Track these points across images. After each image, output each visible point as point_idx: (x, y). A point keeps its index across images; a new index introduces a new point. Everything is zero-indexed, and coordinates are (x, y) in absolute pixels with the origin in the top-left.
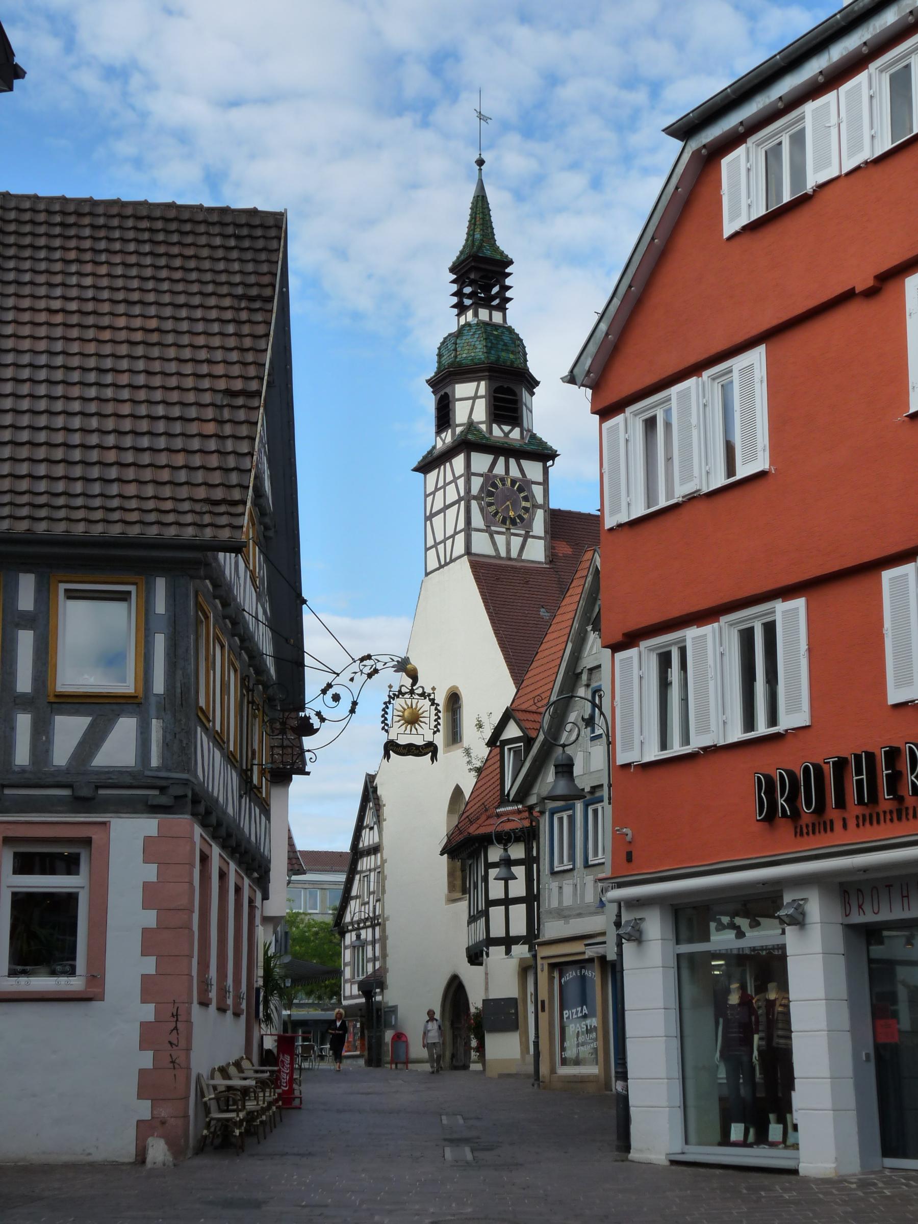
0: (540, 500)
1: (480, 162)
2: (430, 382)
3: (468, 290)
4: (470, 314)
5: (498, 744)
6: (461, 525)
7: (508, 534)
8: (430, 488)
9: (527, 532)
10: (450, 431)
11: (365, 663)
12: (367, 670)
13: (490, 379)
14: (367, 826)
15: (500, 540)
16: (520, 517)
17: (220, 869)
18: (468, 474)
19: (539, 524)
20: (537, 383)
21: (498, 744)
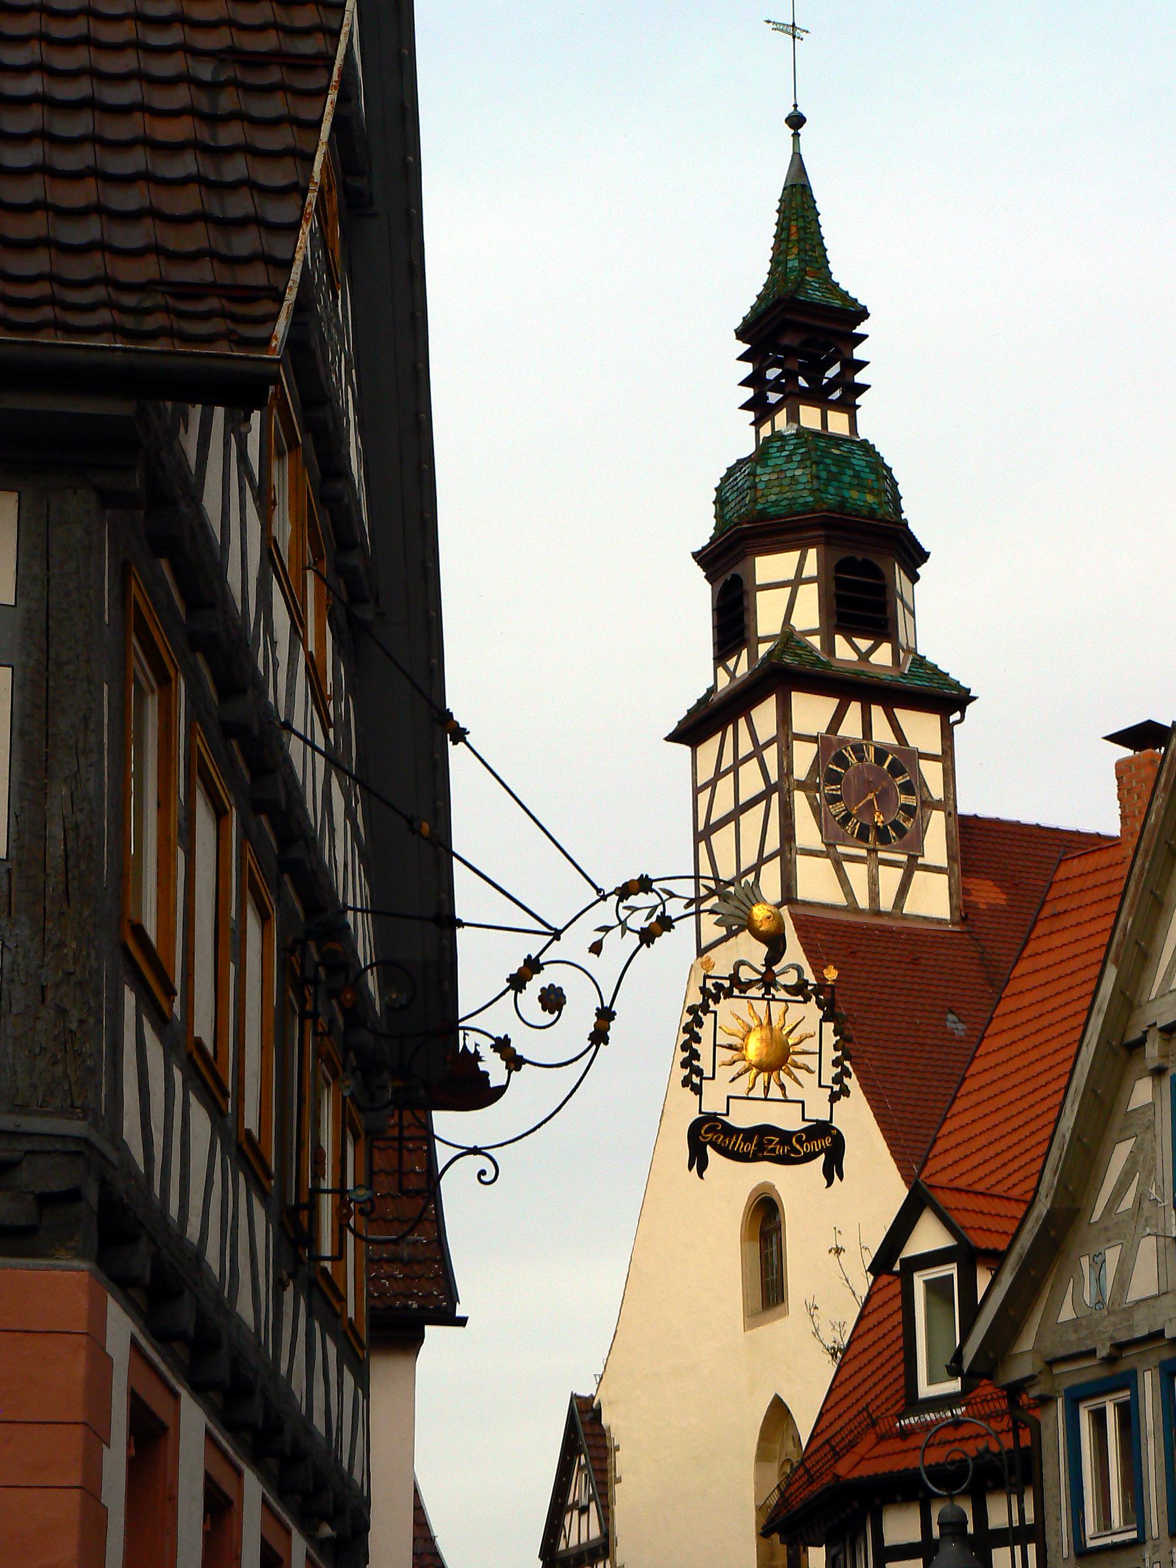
0: (937, 791)
1: (796, 121)
2: (701, 557)
3: (772, 373)
4: (781, 418)
5: (897, 1267)
6: (773, 842)
7: (874, 862)
8: (706, 773)
9: (913, 858)
10: (745, 652)
11: (633, 901)
12: (638, 921)
13: (826, 545)
14: (575, 1505)
15: (857, 874)
16: (896, 825)
17: (210, 1483)
18: (786, 736)
19: (936, 845)
20: (924, 556)
21: (897, 1267)
